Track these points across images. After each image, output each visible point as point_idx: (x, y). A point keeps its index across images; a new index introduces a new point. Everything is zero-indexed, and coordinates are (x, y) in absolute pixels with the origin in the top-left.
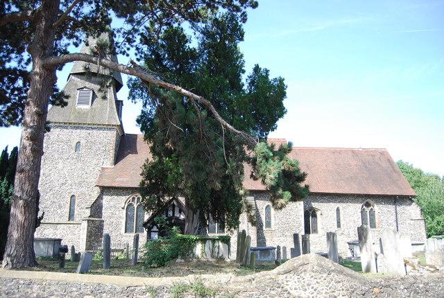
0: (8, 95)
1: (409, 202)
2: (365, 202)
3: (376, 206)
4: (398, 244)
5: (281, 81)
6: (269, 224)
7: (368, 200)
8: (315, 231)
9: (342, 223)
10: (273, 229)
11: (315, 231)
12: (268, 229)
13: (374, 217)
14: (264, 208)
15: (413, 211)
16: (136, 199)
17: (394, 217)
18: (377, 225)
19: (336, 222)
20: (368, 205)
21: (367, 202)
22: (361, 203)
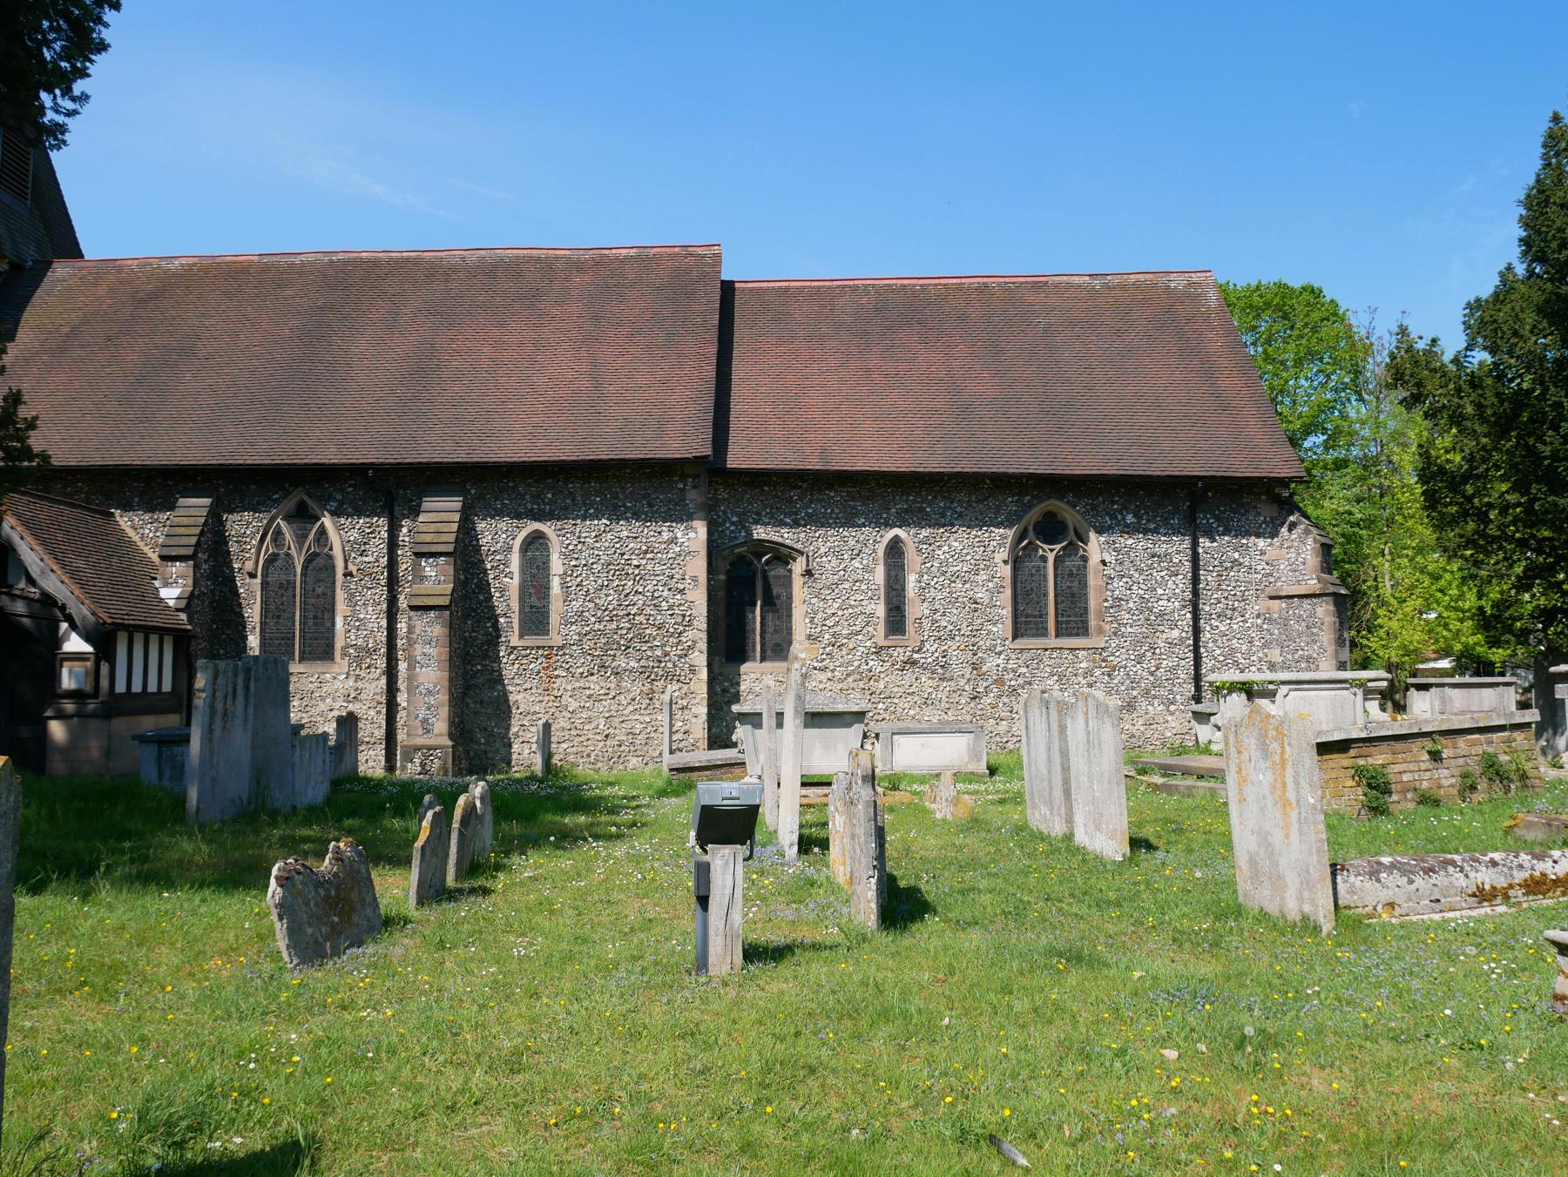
0: (47, 55)
1: (1267, 511)
2: (1033, 515)
3: (1096, 547)
4: (1228, 730)
5: (89, 76)
6: (535, 620)
7: (1054, 504)
8: (778, 649)
9: (915, 610)
10: (556, 639)
11: (778, 649)
12: (531, 641)
13: (1084, 585)
14: (517, 544)
15: (1289, 557)
16: (1207, 968)
17: (1181, 584)
18: (1093, 623)
19: (880, 610)
20: (1051, 529)
21: (1050, 516)
22: (1006, 524)
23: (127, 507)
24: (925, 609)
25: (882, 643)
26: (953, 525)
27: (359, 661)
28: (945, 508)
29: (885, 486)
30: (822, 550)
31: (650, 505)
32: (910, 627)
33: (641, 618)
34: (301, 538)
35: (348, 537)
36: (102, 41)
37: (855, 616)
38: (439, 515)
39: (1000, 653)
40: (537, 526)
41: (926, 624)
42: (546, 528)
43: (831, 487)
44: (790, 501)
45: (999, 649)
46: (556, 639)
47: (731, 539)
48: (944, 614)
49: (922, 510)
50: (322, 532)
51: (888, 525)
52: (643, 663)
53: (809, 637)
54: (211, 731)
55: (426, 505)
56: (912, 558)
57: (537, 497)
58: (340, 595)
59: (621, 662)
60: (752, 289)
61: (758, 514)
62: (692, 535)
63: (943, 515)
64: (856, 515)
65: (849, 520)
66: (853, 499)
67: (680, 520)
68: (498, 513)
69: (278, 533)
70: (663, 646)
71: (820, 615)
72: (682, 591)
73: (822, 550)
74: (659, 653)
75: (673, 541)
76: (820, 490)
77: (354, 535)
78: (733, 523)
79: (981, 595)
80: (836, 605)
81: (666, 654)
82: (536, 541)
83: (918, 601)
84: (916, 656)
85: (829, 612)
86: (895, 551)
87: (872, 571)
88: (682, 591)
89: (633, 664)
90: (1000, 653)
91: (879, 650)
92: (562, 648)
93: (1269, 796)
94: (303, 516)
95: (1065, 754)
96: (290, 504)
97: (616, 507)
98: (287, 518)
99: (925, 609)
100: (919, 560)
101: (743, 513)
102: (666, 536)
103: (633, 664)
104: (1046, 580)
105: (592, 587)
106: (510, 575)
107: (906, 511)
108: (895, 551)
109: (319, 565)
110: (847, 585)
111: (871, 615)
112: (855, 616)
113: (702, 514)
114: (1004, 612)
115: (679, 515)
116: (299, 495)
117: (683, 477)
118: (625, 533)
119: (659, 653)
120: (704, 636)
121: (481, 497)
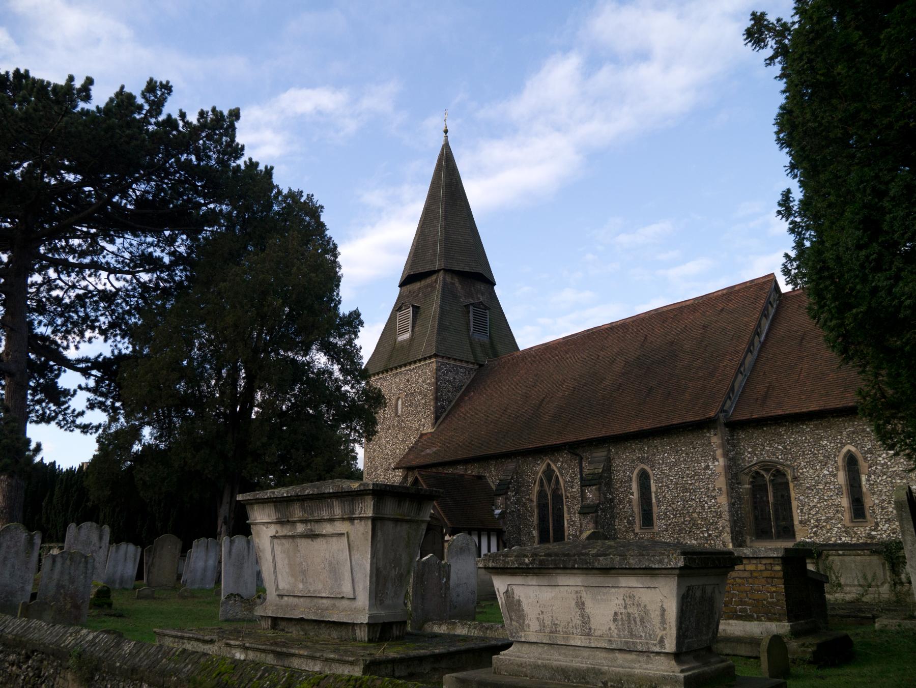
9: (870, 501)
19: (845, 502)
25: (848, 524)
36: (50, 464)
37: (829, 507)
41: (878, 511)
43: (766, 425)
46: (656, 529)
47: (749, 462)
49: (864, 430)
54: (849, 617)
61: (763, 445)
62: (717, 463)
70: (708, 530)
73: (803, 464)
75: (707, 467)
76: (797, 426)
78: (749, 453)
80: (815, 500)
81: (710, 535)
83: (869, 493)
84: (873, 533)
87: (835, 476)
95: (640, 569)
100: (866, 465)
106: (632, 494)
107: (853, 433)
112: (829, 507)
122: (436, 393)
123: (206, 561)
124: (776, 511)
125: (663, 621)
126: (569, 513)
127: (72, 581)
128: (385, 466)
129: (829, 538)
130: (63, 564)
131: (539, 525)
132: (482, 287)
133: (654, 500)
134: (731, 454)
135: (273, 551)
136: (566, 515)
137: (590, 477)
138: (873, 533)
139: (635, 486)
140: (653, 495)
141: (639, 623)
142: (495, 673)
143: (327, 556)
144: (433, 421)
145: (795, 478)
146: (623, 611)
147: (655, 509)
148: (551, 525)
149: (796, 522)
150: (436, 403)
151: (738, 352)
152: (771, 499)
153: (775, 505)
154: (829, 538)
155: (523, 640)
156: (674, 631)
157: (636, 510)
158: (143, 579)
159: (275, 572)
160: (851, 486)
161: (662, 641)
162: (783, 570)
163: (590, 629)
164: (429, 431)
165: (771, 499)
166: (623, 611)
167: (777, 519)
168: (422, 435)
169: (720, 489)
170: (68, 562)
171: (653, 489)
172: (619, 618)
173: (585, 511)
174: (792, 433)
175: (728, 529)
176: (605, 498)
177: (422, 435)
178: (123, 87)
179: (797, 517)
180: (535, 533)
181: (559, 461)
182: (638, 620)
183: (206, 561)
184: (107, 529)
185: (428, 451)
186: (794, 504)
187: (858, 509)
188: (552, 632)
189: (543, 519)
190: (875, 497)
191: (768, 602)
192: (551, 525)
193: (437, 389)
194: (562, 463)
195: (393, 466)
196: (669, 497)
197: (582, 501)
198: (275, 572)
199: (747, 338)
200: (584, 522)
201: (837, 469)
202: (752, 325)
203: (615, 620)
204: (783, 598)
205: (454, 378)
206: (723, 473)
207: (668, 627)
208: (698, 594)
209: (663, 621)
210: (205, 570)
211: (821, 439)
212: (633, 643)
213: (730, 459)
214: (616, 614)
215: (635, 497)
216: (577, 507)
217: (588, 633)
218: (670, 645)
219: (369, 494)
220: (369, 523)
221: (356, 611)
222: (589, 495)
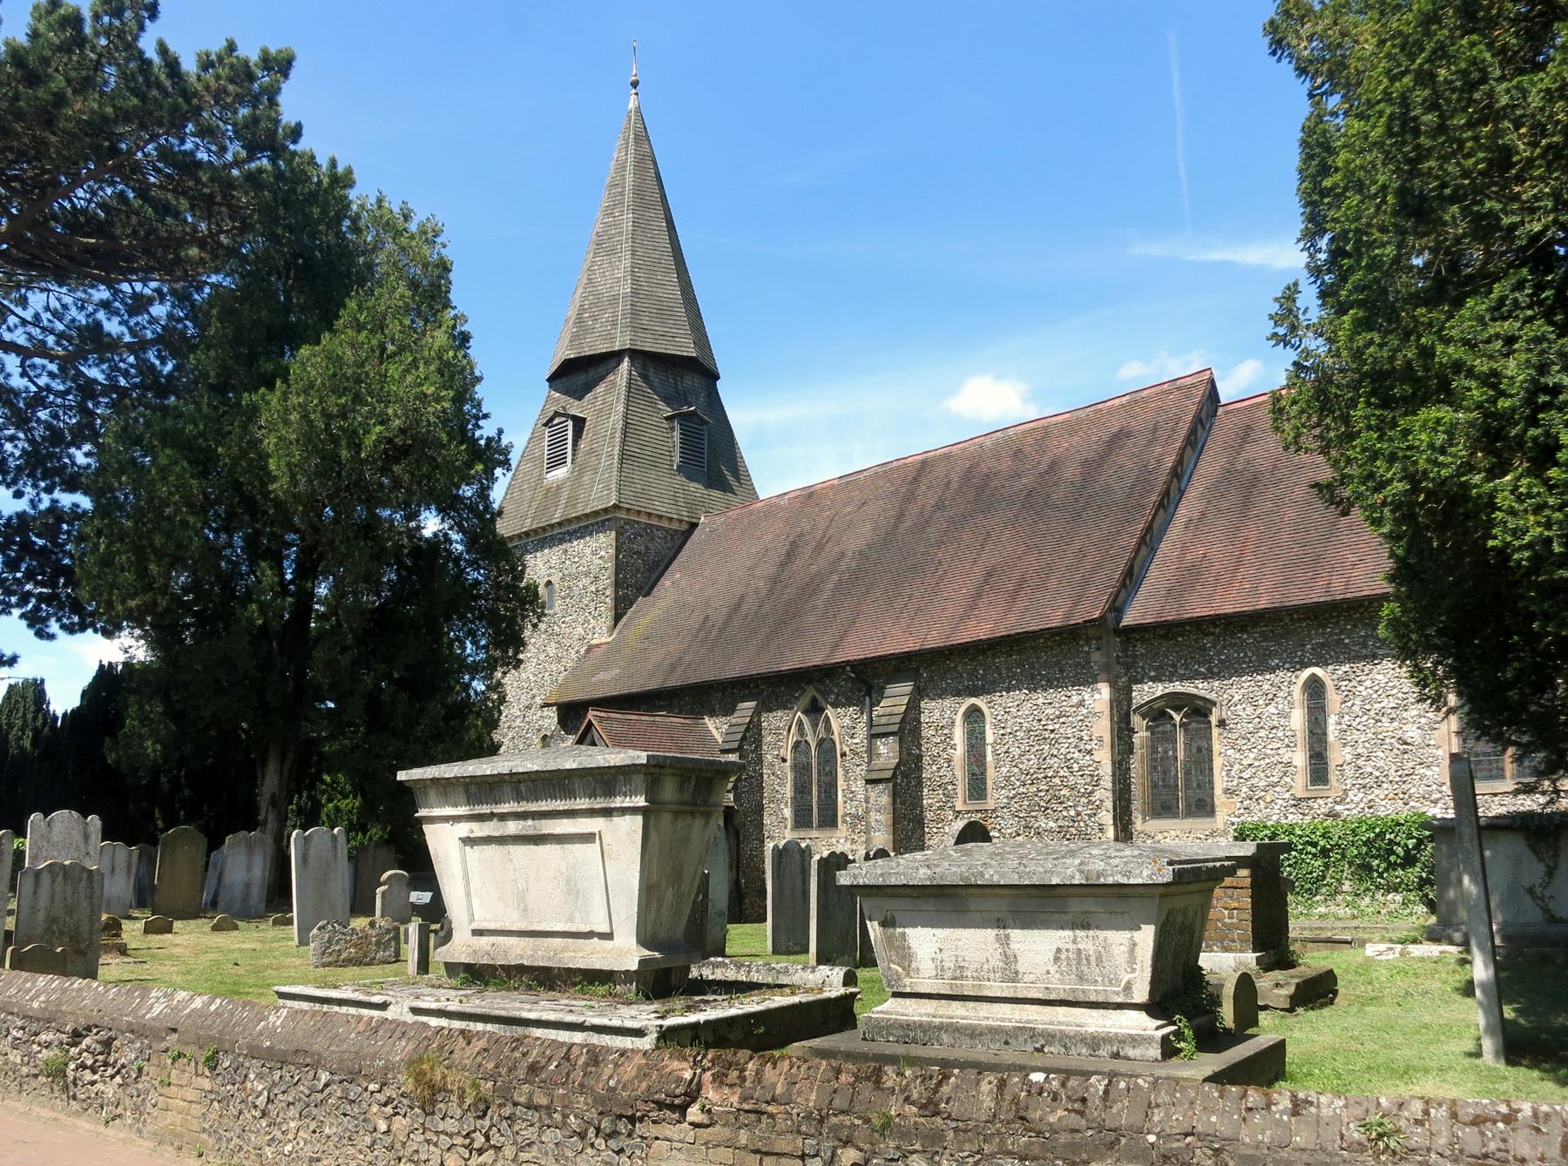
9: (1338, 755)
19: (1300, 758)
23: (713, 714)
24: (1347, 754)
26: (1374, 656)
27: (853, 827)
28: (1366, 637)
29: (1299, 620)
30: (1237, 697)
31: (1061, 671)
32: (1333, 776)
33: (1057, 780)
34: (815, 726)
35: (843, 722)
38: (896, 697)
39: (1435, 802)
40: (973, 700)
42: (980, 702)
43: (1243, 629)
44: (1203, 649)
45: (1435, 796)
46: (990, 804)
48: (1369, 759)
49: (1339, 642)
50: (827, 720)
51: (1305, 666)
52: (1060, 823)
53: (1226, 791)
55: (888, 692)
56: (1333, 698)
57: (972, 674)
58: (840, 772)
59: (1043, 823)
60: (1245, 408)
61: (1174, 666)
62: (1097, 696)
63: (1365, 646)
64: (1271, 655)
65: (1262, 666)
66: (1266, 639)
67: (1086, 683)
68: (941, 695)
69: (800, 723)
71: (1237, 767)
72: (1090, 752)
73: (1237, 697)
74: (1072, 813)
75: (1081, 704)
77: (847, 721)
79: (1412, 733)
80: (1252, 756)
81: (1078, 814)
82: (974, 715)
84: (1338, 808)
85: (1245, 762)
86: (1315, 689)
87: (1287, 716)
88: (1090, 752)
89: (1051, 824)
90: (1435, 802)
91: (1298, 802)
92: (994, 811)
93: (1053, 969)
94: (814, 710)
96: (805, 701)
97: (1033, 677)
98: (805, 712)
99: (1347, 754)
100: (1339, 699)
101: (1160, 667)
102: (1075, 699)
103: (1051, 824)
104: (810, 794)
105: (1016, 752)
106: (953, 747)
107: (1323, 645)
108: (1315, 689)
109: (827, 747)
110: (1262, 733)
111: (1289, 764)
113: (1104, 676)
114: (1440, 752)
115: (1086, 679)
116: (811, 692)
117: (1088, 640)
118: (1041, 701)
119: (1072, 813)
120: (1110, 795)
121: (931, 679)
122: (617, 574)
123: (249, 869)
124: (1187, 772)
125: (1132, 959)
126: (847, 779)
127: (70, 911)
128: (525, 701)
129: (1268, 817)
130: (53, 882)
131: (794, 799)
132: (691, 381)
133: (989, 758)
134: (413, 524)
135: (464, 862)
136: (840, 782)
137: (883, 720)
138: (1338, 808)
139: (959, 735)
140: (989, 749)
141: (1093, 963)
142: (864, 1039)
143: (563, 869)
144: (610, 623)
145: (1222, 723)
146: (1071, 946)
147: (991, 773)
148: (815, 800)
149: (1218, 791)
150: (616, 592)
151: (1143, 507)
152: (1181, 755)
153: (1185, 763)
154: (1268, 817)
155: (908, 990)
156: (1147, 974)
157: (959, 773)
158: (807, 951)
159: (468, 895)
160: (1311, 732)
161: (1128, 988)
162: (1252, 876)
163: (1017, 973)
164: (603, 640)
165: (1181, 755)
166: (1071, 946)
167: (1187, 787)
168: (590, 649)
169: (1100, 739)
170: (60, 879)
171: (990, 737)
172: (1063, 956)
173: (875, 776)
174: (1224, 647)
175: (1109, 804)
176: (909, 754)
177: (590, 649)
178: (281, 65)
179: (1220, 782)
180: (787, 812)
181: (831, 692)
182: (1093, 959)
183: (249, 869)
184: (94, 821)
185: (602, 676)
186: (1218, 762)
187: (1319, 769)
188: (955, 978)
189: (801, 789)
190: (1348, 749)
191: (1224, 924)
192: (815, 800)
193: (619, 567)
194: (837, 695)
195: (538, 700)
196: (1016, 752)
197: (869, 763)
198: (468, 895)
199: (1159, 487)
200: (873, 795)
201: (1291, 705)
202: (1169, 461)
203: (1057, 959)
204: (1248, 916)
205: (647, 548)
206: (1107, 712)
207: (1137, 967)
208: (1179, 919)
209: (1132, 959)
210: (248, 886)
211: (1270, 655)
212: (1084, 992)
213: (1118, 690)
214: (1059, 950)
215: (959, 750)
216: (861, 771)
217: (1014, 977)
218: (1141, 994)
219: (638, 772)
220: (639, 819)
221: (621, 954)
222: (883, 749)
